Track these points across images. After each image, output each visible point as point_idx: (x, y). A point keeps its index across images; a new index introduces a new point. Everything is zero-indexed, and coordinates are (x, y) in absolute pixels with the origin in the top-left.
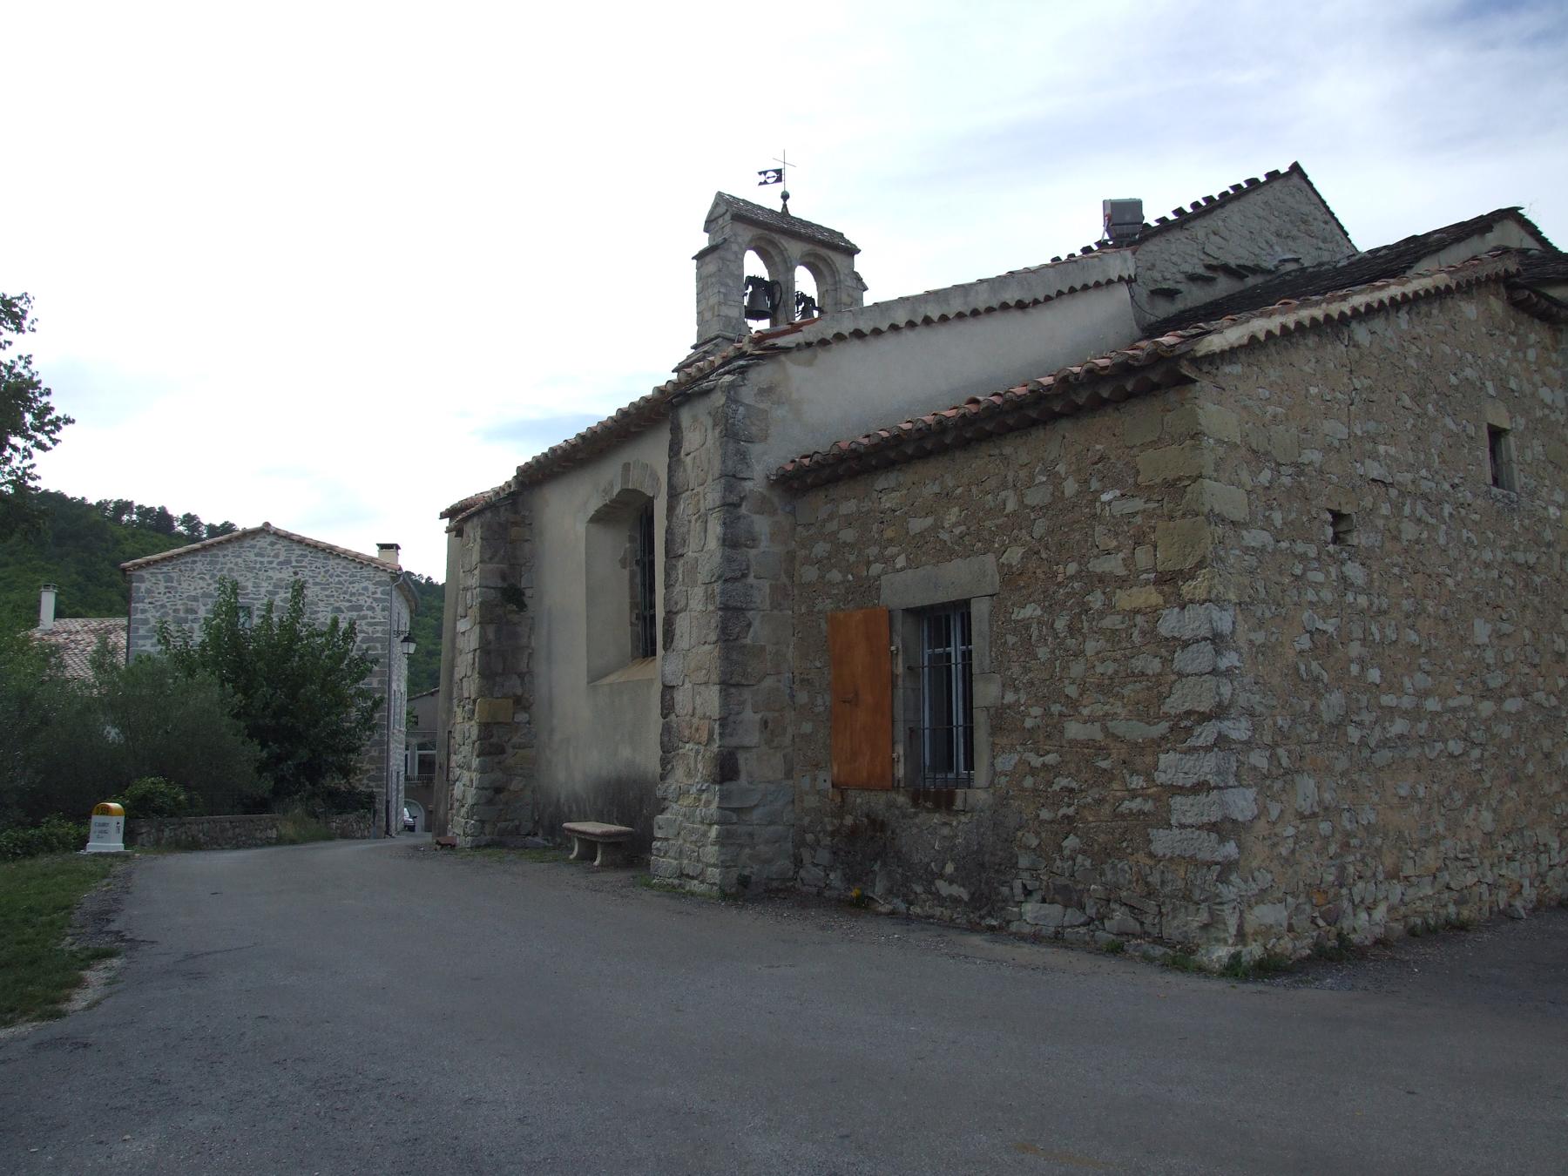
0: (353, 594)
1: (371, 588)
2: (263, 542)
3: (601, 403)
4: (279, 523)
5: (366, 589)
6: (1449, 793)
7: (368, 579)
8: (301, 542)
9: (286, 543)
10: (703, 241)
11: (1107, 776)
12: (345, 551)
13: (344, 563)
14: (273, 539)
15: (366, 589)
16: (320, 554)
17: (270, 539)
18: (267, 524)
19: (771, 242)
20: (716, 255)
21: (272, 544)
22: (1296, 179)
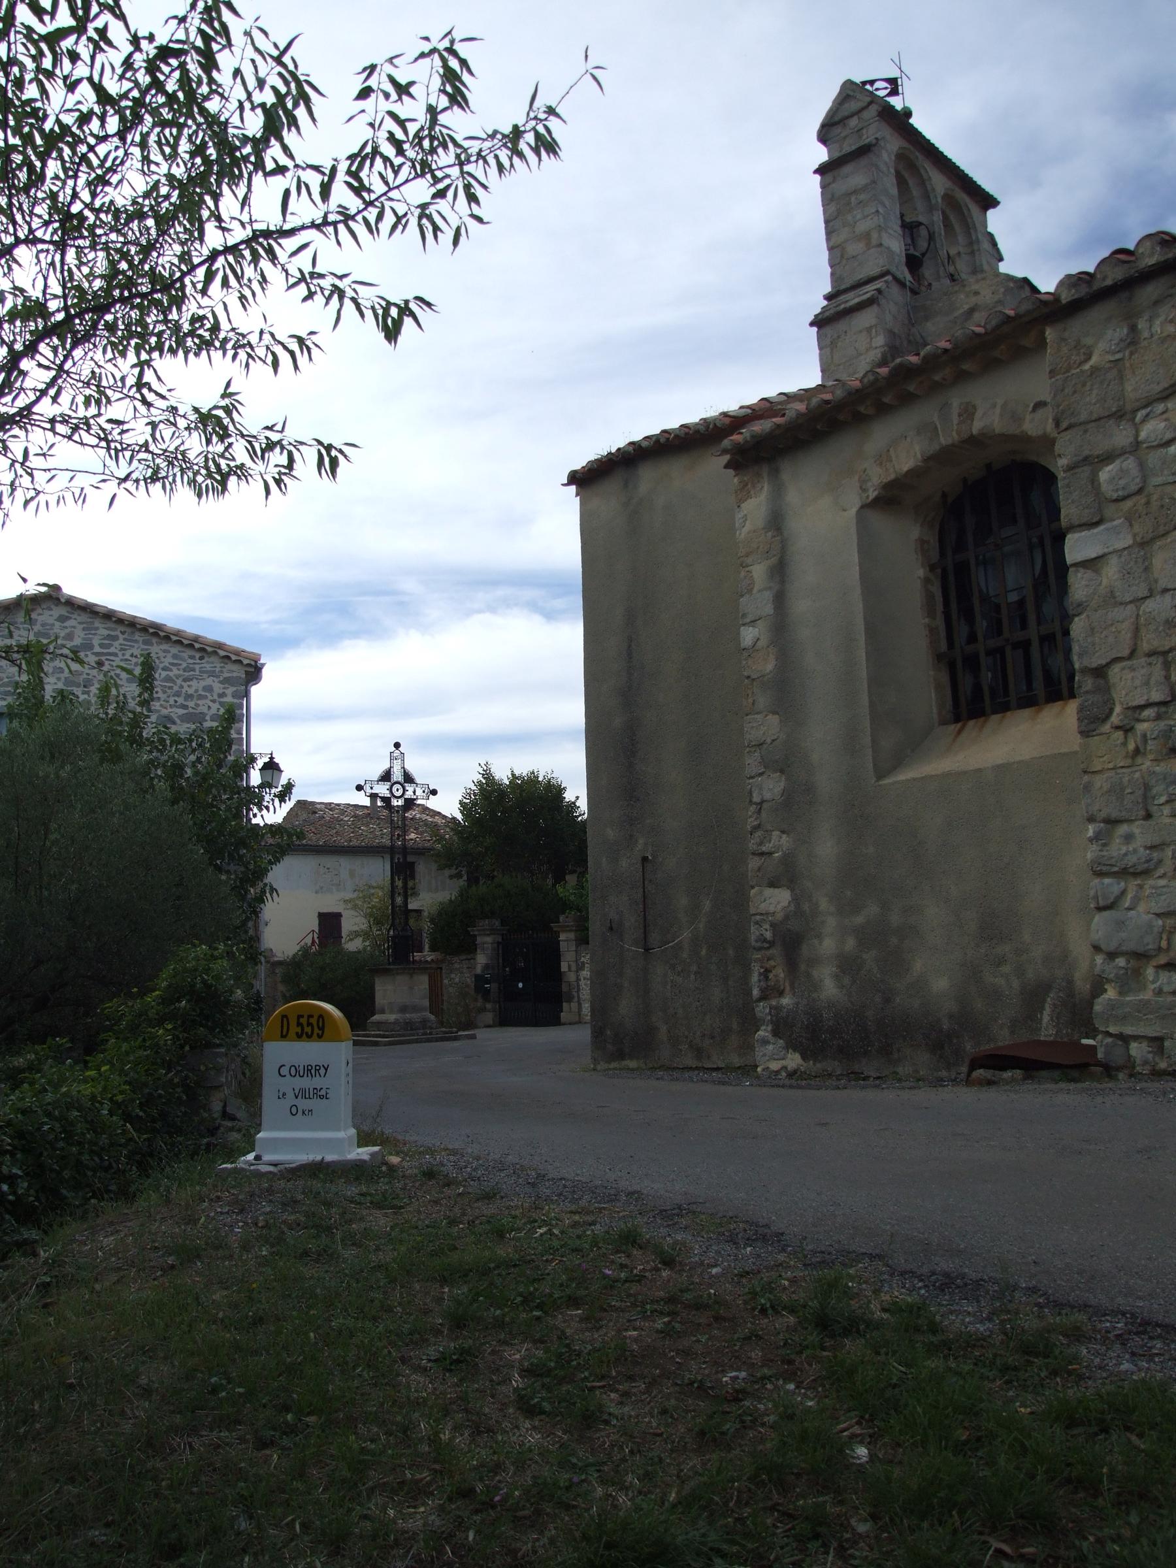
0: (189, 697)
1: (218, 688)
2: (46, 616)
3: (999, 246)
4: (71, 589)
5: (209, 689)
6: (466, 1411)
7: (212, 674)
8: (109, 616)
9: (84, 617)
10: (821, 154)
11: (569, 1362)
12: (178, 633)
13: (175, 650)
14: (63, 611)
15: (209, 689)
16: (137, 636)
17: (58, 611)
18: (56, 588)
19: (912, 167)
20: (864, 161)
21: (63, 619)
22: (239, 672)
